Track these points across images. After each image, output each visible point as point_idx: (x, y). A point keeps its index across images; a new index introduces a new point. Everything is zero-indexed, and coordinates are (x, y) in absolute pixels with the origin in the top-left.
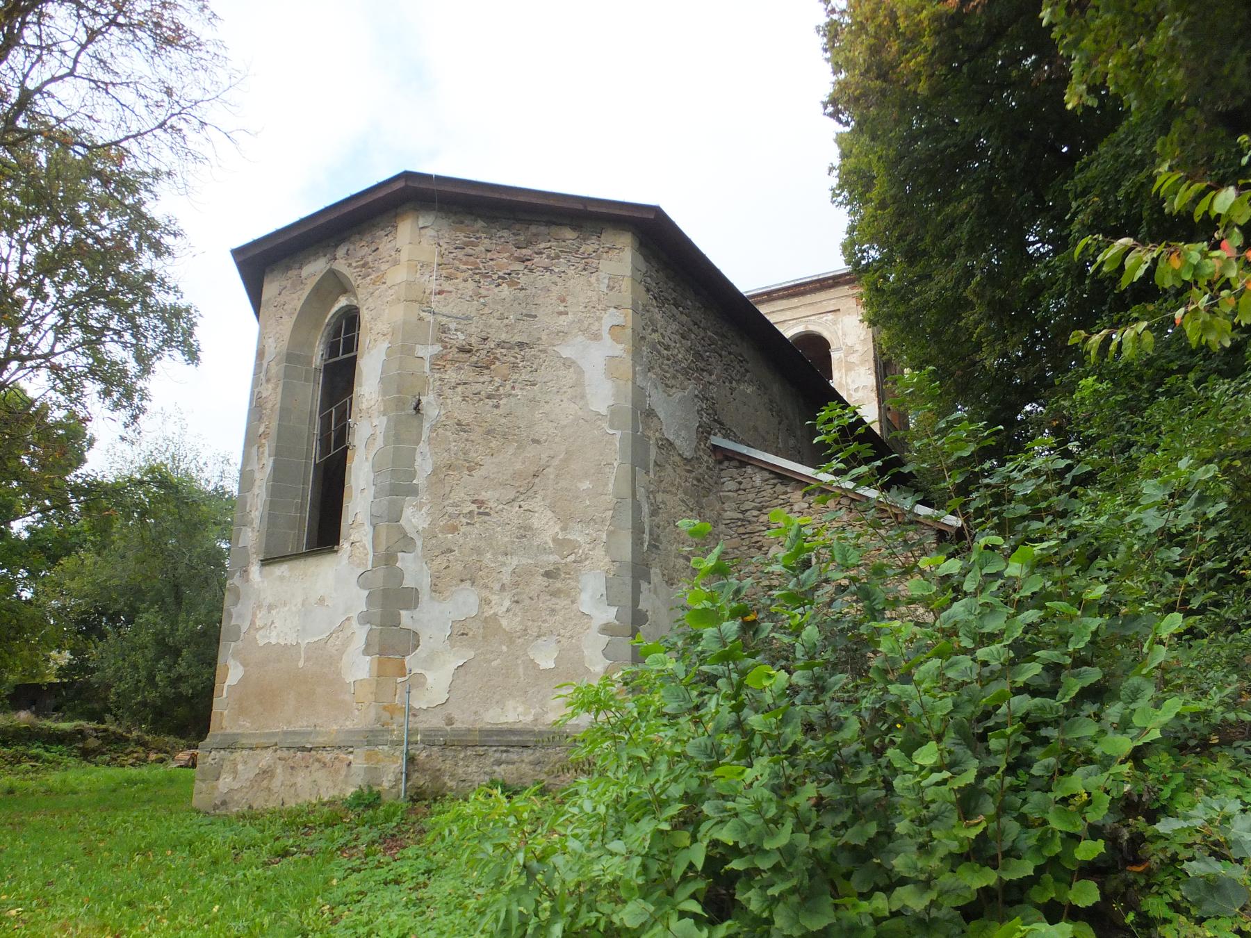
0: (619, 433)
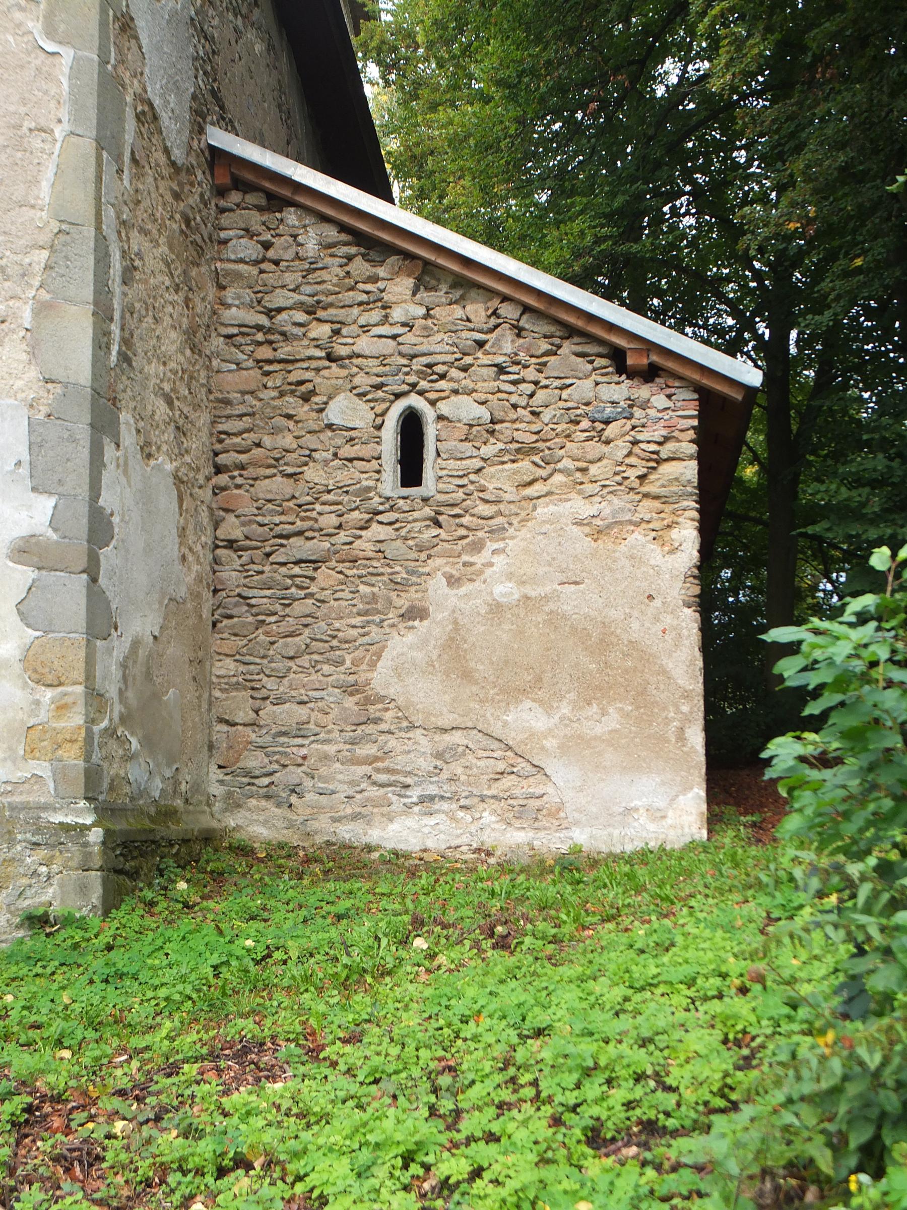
0: (68, 54)
